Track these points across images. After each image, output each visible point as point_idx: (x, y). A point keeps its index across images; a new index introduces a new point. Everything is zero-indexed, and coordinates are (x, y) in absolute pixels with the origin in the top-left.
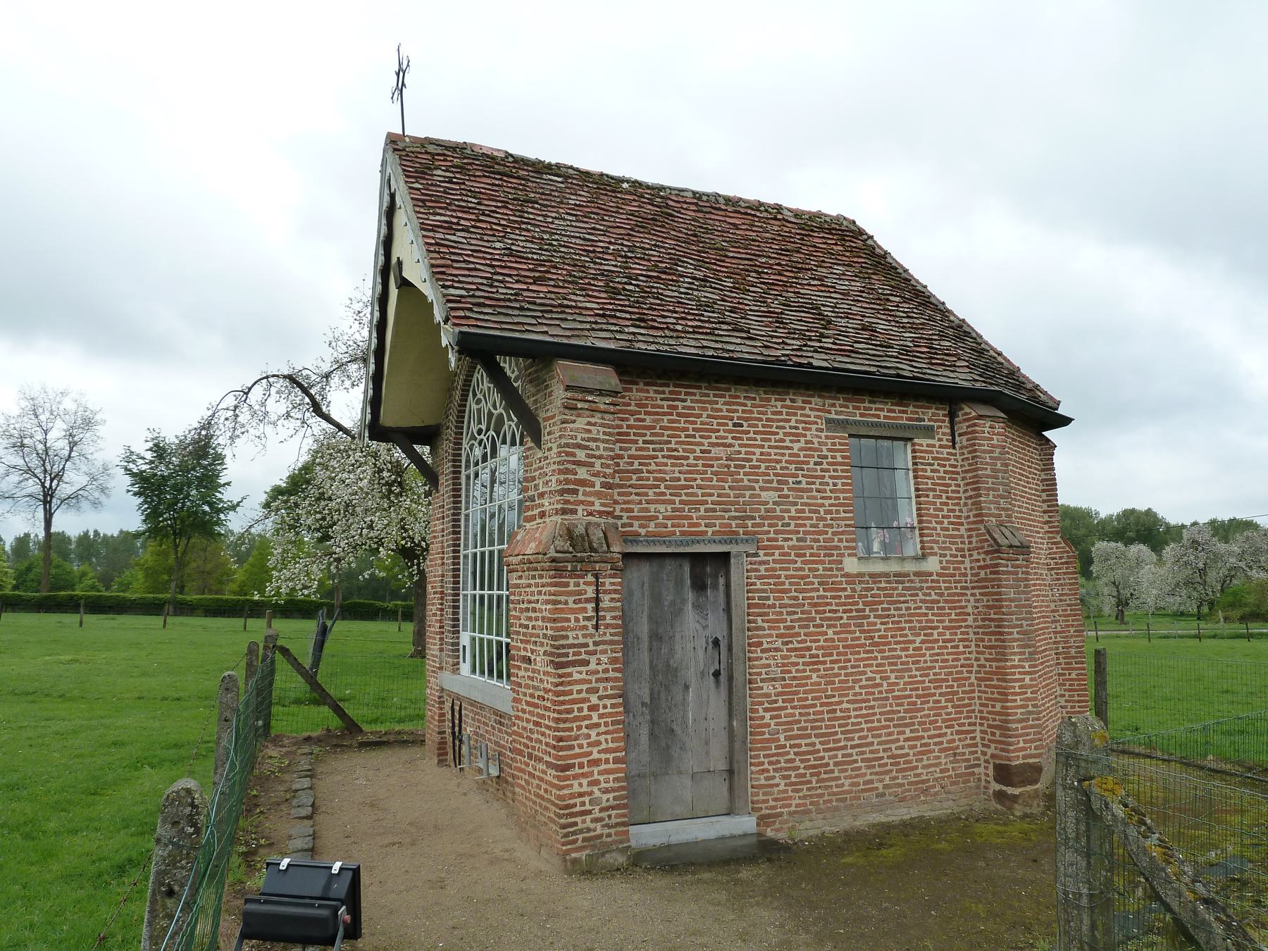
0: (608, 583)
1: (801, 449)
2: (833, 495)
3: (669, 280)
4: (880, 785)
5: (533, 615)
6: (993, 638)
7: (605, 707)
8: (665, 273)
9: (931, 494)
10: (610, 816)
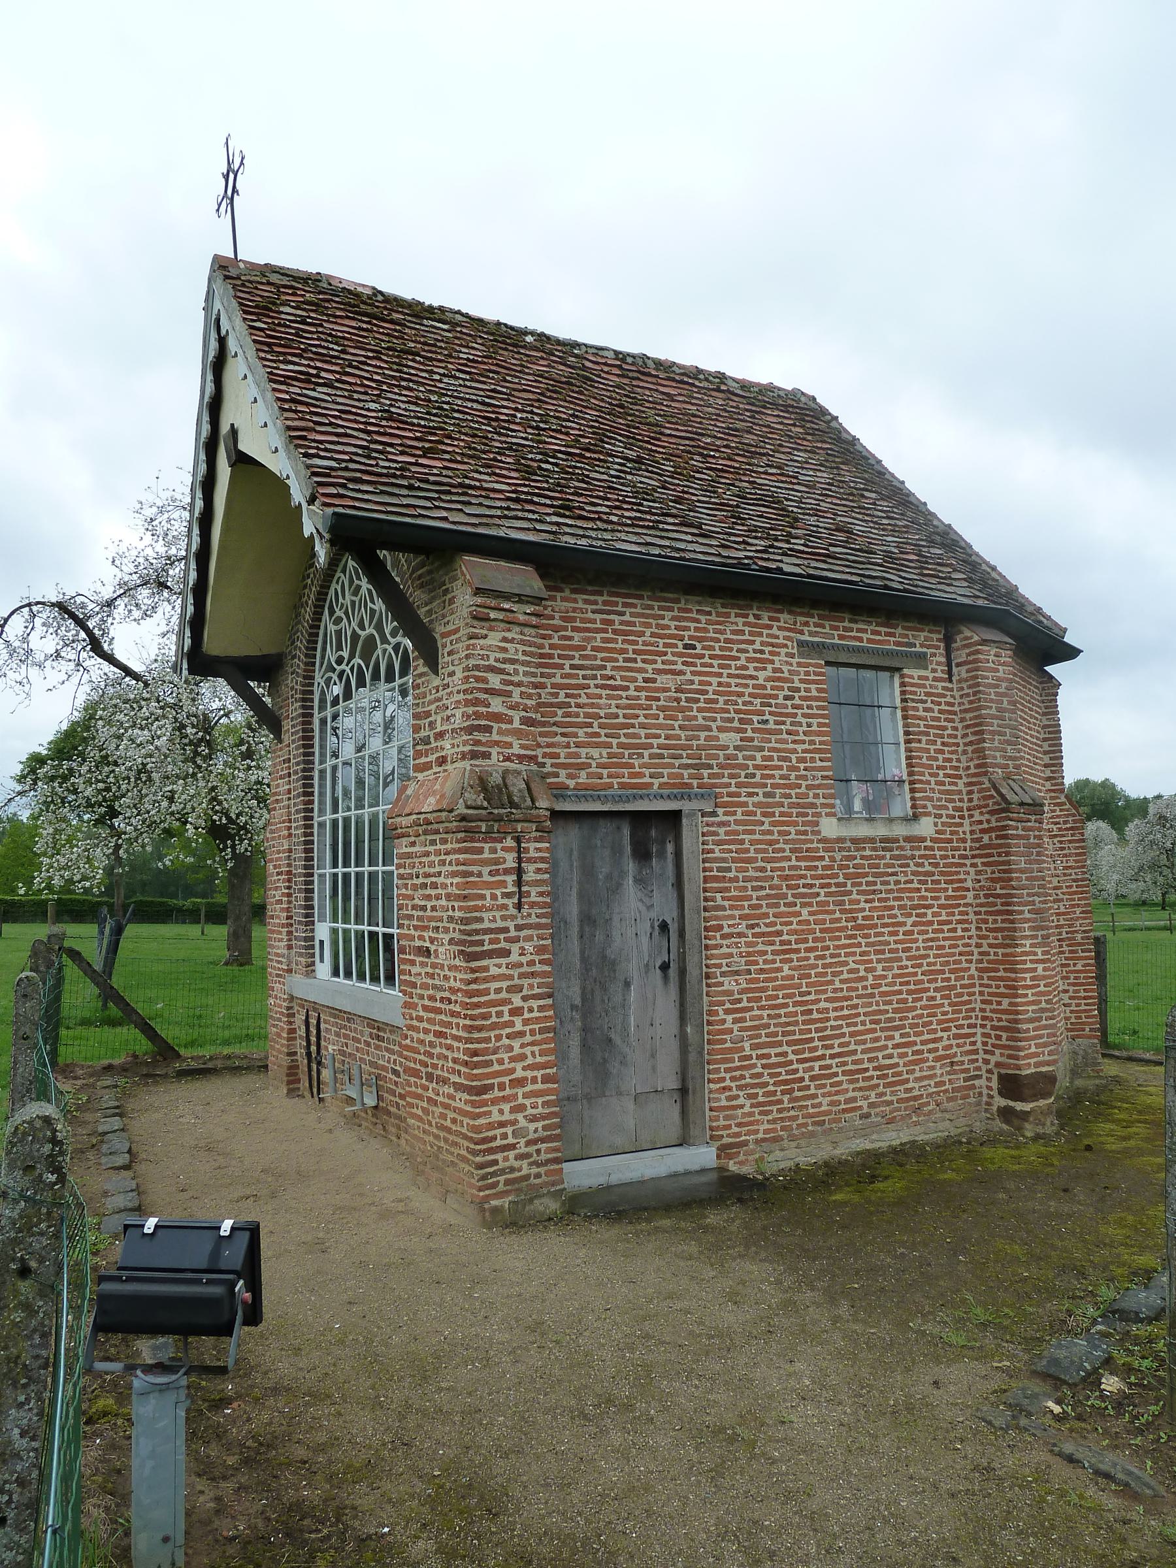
0: (533, 848)
1: (768, 679)
2: (807, 739)
3: (595, 459)
4: (864, 1104)
5: (433, 892)
6: (999, 918)
7: (531, 1010)
8: (588, 450)
9: (924, 739)
10: (538, 1151)
